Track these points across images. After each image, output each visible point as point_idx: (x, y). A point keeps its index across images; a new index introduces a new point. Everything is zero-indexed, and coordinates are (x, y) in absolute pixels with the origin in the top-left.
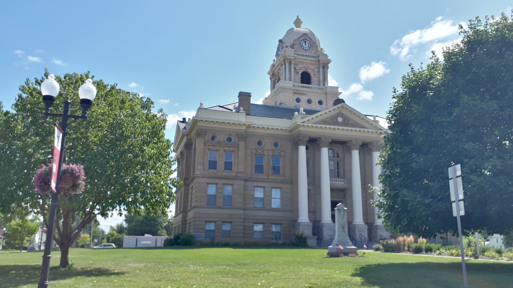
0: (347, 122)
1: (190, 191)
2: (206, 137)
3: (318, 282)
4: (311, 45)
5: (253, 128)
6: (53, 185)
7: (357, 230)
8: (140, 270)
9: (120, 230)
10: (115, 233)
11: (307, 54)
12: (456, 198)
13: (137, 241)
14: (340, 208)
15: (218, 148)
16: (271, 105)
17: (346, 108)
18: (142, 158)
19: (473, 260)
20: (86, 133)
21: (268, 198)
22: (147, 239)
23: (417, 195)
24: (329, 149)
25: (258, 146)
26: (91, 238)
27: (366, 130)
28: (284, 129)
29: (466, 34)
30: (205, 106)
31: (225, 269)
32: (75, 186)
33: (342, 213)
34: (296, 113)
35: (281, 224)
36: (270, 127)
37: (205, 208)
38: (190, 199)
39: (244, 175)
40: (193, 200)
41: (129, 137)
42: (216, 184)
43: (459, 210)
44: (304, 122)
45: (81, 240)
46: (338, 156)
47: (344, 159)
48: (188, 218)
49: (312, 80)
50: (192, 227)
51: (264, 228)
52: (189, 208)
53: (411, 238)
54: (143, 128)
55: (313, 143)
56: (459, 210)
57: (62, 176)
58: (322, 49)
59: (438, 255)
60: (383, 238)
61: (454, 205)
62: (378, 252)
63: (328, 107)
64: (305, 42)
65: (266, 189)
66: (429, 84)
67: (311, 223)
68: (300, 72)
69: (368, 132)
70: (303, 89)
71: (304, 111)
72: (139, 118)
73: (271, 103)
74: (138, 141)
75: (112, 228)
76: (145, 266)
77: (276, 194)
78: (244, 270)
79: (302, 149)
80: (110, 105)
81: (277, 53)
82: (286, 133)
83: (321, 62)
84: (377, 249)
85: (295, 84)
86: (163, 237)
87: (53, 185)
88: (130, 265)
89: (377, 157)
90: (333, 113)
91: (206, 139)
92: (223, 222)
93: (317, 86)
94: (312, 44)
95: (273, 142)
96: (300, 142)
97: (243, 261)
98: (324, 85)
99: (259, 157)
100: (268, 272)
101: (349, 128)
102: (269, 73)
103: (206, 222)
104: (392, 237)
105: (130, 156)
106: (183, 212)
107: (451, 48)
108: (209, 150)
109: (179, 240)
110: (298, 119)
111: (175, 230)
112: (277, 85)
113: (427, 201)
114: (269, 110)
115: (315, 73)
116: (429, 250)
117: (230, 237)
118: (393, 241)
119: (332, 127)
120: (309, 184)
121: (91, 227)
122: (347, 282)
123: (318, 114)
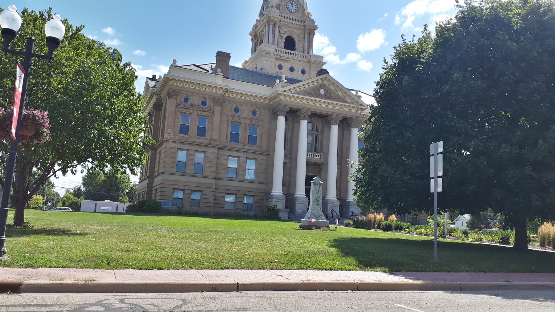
0: (329, 95)
1: (158, 155)
2: (179, 98)
3: (294, 250)
4: (297, 8)
5: (230, 93)
6: (13, 131)
7: (329, 205)
8: (105, 232)
9: (77, 193)
10: (71, 196)
11: (292, 17)
12: (435, 174)
13: (96, 206)
14: (316, 181)
15: (191, 111)
16: (251, 69)
17: (329, 80)
18: (111, 111)
19: (440, 239)
20: (49, 78)
21: (241, 169)
22: (107, 205)
23: (396, 171)
24: (308, 122)
25: (235, 113)
26: (45, 201)
27: (348, 105)
28: (264, 97)
29: (461, 9)
30: (179, 64)
31: (197, 235)
32: (39, 134)
33: (318, 187)
34: (278, 81)
35: (253, 196)
36: (239, 92)
37: (173, 174)
38: (157, 164)
39: (218, 143)
40: (161, 166)
41: (97, 87)
42: (187, 150)
43: (436, 186)
44: (285, 91)
45: (32, 202)
46: (317, 130)
47: (322, 133)
48: (154, 185)
49: (296, 47)
50: (158, 194)
51: (236, 198)
52: (156, 174)
53: (381, 216)
54: (112, 78)
55: (293, 115)
56: (436, 186)
57: (23, 121)
58: (309, 13)
59: (408, 233)
60: (354, 214)
61: (432, 181)
62: (349, 228)
63: (311, 77)
64: (292, 4)
65: (241, 159)
66: (419, 57)
67: (284, 197)
68: (285, 37)
69: (349, 106)
70: (284, 55)
71: (286, 79)
72: (109, 67)
73: (250, 67)
74: (107, 91)
75: (67, 191)
76: (110, 229)
77: (251, 165)
78: (217, 237)
79: (281, 120)
80: (76, 48)
81: (261, 12)
82: (266, 101)
83: (307, 27)
84: (348, 225)
85: (278, 49)
86: (124, 205)
87: (13, 131)
88: (92, 227)
89: (356, 134)
90: (316, 84)
91: (179, 100)
92: (192, 191)
93: (302, 54)
94: (299, 6)
95: (251, 111)
96: (280, 112)
97: (215, 229)
98: (308, 53)
99: (236, 125)
100: (242, 240)
101: (331, 102)
102: (250, 34)
103: (174, 189)
104: (363, 214)
105: (98, 108)
106: (148, 177)
107: (444, 23)
108: (181, 112)
109: (144, 207)
110: (279, 87)
111: (139, 196)
112: (259, 48)
113: (406, 178)
114: (248, 75)
115: (300, 39)
116: (398, 228)
117: (199, 207)
118: (364, 218)
119: (314, 99)
120: (285, 157)
121: (44, 190)
122: (322, 251)
123: (300, 84)
